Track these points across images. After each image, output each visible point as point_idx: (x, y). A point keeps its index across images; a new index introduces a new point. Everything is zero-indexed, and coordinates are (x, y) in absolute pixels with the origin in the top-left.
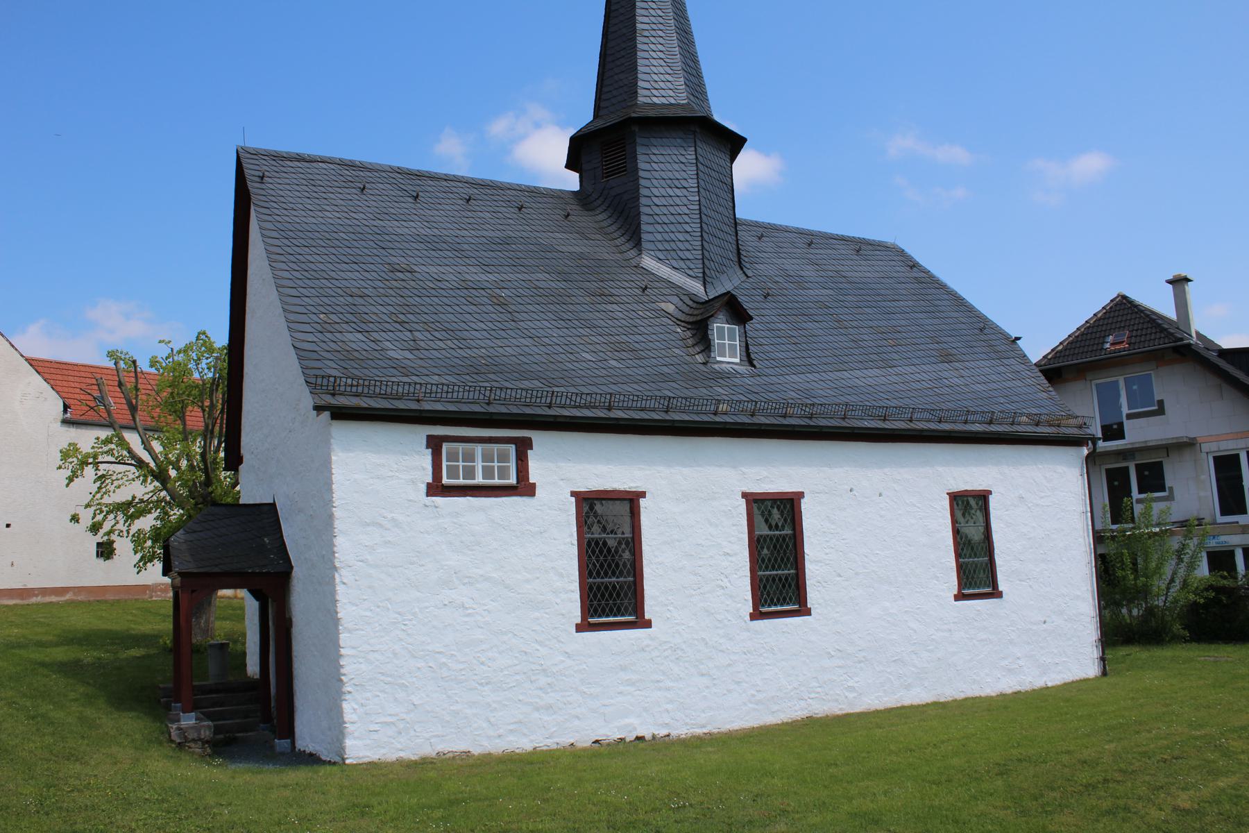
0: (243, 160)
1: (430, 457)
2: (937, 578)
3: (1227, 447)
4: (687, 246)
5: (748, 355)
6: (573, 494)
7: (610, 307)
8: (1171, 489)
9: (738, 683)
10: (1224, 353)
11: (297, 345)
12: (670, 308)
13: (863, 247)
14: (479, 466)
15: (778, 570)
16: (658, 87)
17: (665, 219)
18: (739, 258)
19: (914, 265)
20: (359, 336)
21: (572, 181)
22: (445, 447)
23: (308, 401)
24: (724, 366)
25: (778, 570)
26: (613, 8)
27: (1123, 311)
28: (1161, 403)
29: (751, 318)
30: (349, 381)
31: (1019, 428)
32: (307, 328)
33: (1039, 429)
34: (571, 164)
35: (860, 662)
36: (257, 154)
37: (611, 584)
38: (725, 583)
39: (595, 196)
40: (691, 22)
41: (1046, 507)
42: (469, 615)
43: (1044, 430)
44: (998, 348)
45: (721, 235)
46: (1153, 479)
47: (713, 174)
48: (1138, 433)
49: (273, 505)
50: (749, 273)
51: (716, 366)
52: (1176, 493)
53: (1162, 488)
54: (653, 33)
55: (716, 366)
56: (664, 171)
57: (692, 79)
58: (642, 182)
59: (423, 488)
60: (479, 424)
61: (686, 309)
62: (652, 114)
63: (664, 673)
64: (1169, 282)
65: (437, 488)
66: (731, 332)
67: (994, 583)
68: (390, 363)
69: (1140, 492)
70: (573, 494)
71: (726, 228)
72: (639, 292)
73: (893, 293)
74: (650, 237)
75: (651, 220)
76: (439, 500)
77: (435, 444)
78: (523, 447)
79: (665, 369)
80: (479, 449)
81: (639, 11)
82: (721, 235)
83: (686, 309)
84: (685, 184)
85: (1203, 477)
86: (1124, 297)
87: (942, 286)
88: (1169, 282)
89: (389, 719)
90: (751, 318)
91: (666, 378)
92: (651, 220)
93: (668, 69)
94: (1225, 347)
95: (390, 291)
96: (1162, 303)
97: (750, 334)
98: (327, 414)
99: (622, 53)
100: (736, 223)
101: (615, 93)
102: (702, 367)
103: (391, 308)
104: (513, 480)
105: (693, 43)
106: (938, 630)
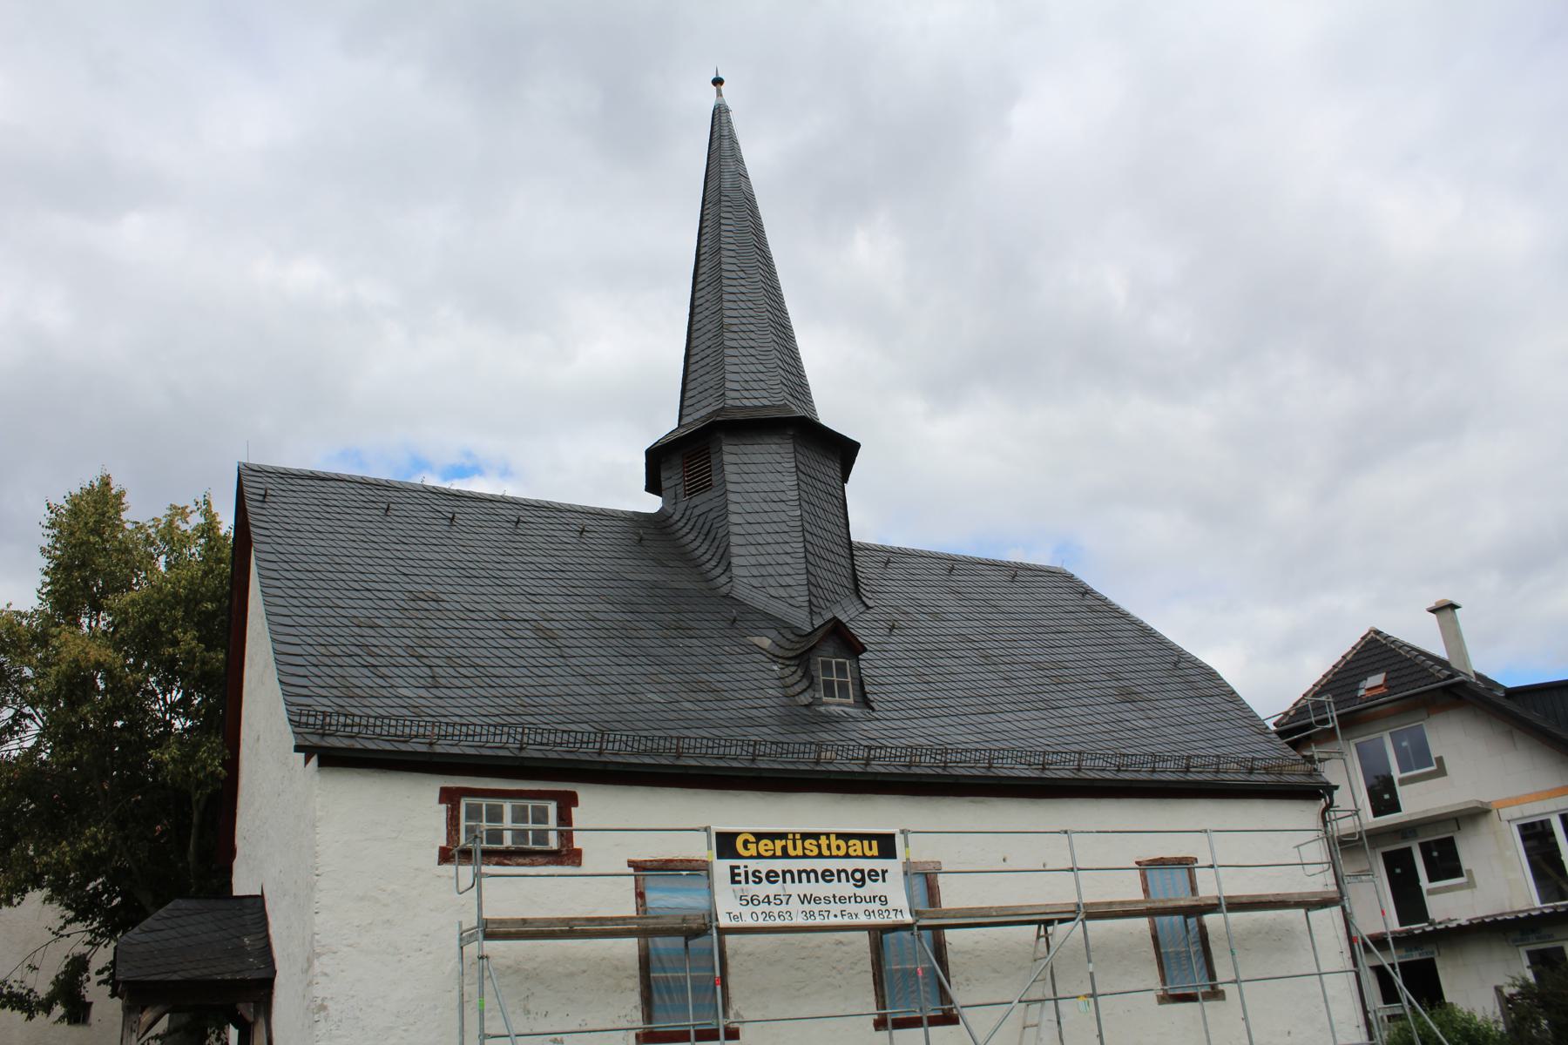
3: (1533, 811)
7: (687, 642)
8: (1470, 872)
10: (1512, 693)
11: (285, 679)
12: (766, 643)
18: (857, 586)
19: (1086, 592)
21: (652, 504)
22: (464, 802)
23: (291, 741)
27: (1375, 651)
28: (1440, 760)
29: (865, 650)
30: (342, 719)
31: (1226, 777)
32: (299, 661)
33: (1253, 777)
34: (653, 486)
43: (1259, 778)
44: (1199, 685)
45: (832, 557)
46: (1446, 863)
47: (819, 485)
48: (1417, 801)
49: (262, 897)
51: (822, 709)
52: (1477, 878)
53: (1456, 871)
55: (822, 709)
61: (787, 645)
62: (740, 416)
64: (1433, 611)
69: (1431, 880)
73: (1050, 618)
74: (742, 561)
77: (449, 797)
78: (567, 802)
80: (507, 807)
82: (832, 557)
83: (787, 645)
85: (1508, 853)
86: (1378, 633)
87: (1125, 616)
88: (1433, 611)
91: (753, 722)
94: (1509, 686)
95: (410, 622)
96: (1425, 636)
102: (805, 711)
103: (408, 641)
104: (554, 843)
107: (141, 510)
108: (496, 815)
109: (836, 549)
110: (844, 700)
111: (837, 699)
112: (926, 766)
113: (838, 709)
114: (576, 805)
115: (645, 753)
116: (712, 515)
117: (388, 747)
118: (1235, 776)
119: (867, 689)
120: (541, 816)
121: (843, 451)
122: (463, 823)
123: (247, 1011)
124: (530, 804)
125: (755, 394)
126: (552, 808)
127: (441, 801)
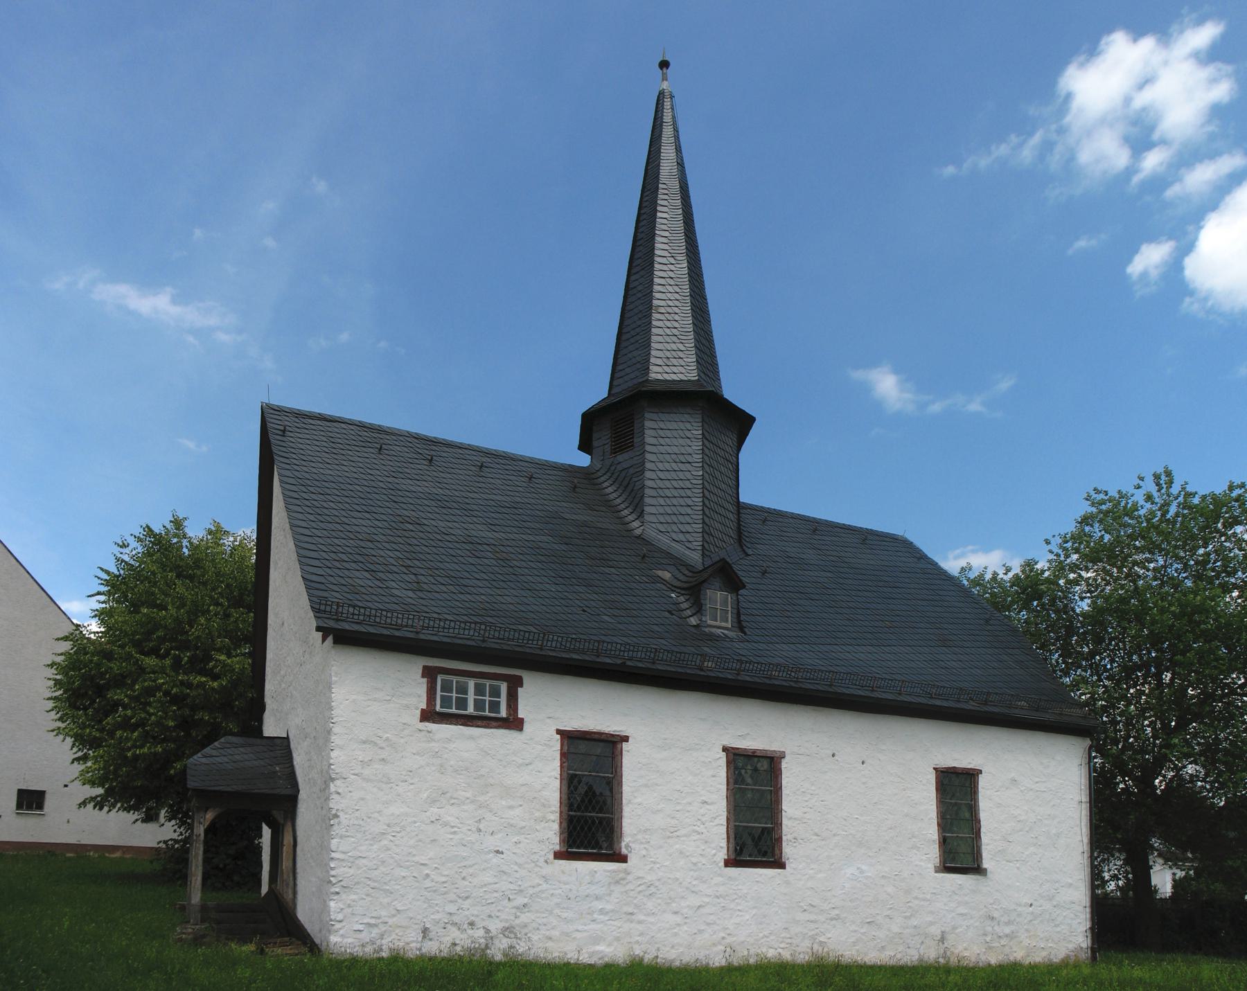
0: (266, 415)
1: (425, 686)
4: (688, 519)
5: (739, 622)
6: (559, 732)
7: (607, 570)
9: (708, 924)
12: (667, 575)
13: (870, 537)
14: (471, 697)
15: (755, 839)
16: (671, 363)
17: (668, 493)
24: (713, 630)
26: (631, 286)
35: (832, 919)
36: (279, 410)
37: (590, 826)
38: (701, 828)
39: (603, 471)
40: (709, 301)
41: (1039, 794)
42: (455, 833)
45: (722, 511)
50: (750, 552)
54: (669, 310)
56: (672, 444)
57: (705, 357)
58: (648, 456)
59: (722, 864)
60: (472, 667)
63: (636, 906)
65: (428, 715)
66: (725, 602)
67: (976, 855)
68: (393, 600)
70: (559, 732)
71: (729, 498)
72: (637, 564)
74: (652, 510)
75: (653, 493)
77: (430, 673)
79: (656, 628)
81: (656, 288)
82: (722, 511)
89: (373, 921)
90: (744, 587)
92: (653, 493)
93: (672, 261)
97: (742, 604)
98: (330, 639)
99: (638, 330)
101: (628, 370)
102: (693, 630)
104: (503, 713)
106: (916, 898)
107: (557, 848)
108: (463, 690)
114: (521, 686)
120: (496, 692)
121: (741, 423)
122: (439, 693)
123: (278, 815)
124: (488, 683)
125: (674, 369)
126: (504, 687)
127: (423, 676)
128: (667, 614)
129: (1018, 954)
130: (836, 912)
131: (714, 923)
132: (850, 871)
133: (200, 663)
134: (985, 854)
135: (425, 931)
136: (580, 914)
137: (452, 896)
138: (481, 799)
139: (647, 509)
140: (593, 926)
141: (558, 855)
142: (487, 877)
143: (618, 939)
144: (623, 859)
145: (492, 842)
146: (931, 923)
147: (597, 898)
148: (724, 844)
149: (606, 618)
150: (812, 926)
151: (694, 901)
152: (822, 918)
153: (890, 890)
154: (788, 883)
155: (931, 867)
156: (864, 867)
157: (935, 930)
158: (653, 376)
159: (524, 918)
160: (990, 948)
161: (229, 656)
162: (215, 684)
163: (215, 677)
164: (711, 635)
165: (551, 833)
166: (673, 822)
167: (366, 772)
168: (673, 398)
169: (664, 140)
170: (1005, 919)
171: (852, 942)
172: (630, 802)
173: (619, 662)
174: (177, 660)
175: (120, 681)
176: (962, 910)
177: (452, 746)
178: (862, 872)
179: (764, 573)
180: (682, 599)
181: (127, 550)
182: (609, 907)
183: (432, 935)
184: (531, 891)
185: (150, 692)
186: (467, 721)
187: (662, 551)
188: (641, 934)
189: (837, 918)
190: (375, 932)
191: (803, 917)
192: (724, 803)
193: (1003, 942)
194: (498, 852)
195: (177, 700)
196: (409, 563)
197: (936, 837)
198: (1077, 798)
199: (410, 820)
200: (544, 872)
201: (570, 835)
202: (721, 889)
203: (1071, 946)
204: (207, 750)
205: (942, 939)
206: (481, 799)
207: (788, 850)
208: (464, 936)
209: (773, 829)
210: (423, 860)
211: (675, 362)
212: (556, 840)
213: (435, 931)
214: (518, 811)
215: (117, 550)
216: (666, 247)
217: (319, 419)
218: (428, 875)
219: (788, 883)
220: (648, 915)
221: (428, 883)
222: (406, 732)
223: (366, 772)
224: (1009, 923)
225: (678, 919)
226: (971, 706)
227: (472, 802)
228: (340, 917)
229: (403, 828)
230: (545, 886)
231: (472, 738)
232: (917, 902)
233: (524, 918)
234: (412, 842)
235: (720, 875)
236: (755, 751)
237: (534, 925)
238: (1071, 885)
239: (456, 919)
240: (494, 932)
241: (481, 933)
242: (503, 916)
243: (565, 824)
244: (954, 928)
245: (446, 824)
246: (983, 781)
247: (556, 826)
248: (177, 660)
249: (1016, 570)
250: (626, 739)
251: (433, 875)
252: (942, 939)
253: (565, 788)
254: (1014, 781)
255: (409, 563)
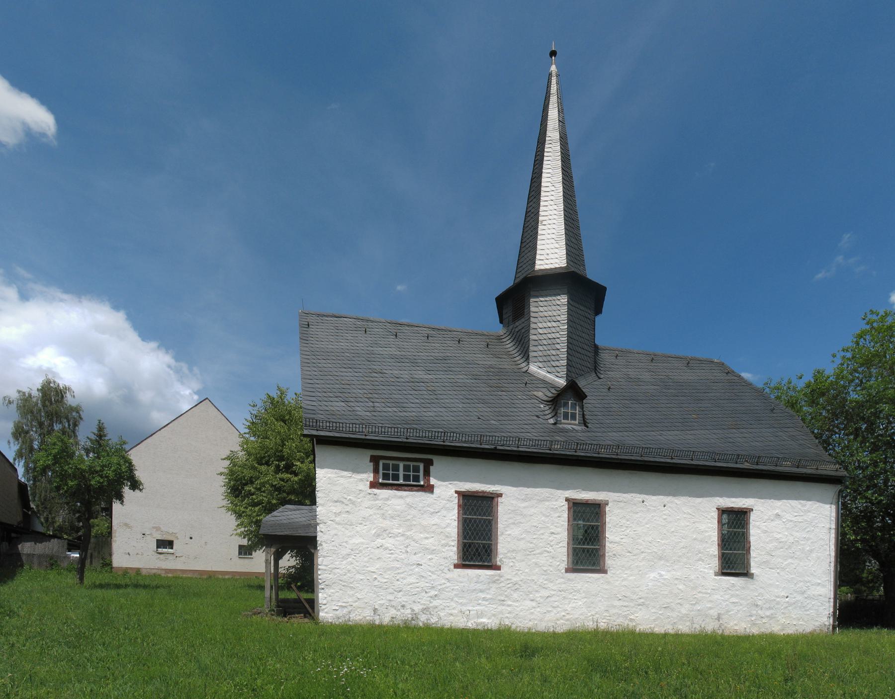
2: (703, 561)
6: (456, 492)
7: (500, 393)
12: (540, 394)
14: (401, 473)
15: (587, 546)
20: (343, 404)
25: (587, 546)
32: (314, 399)
35: (639, 605)
37: (477, 546)
38: (550, 549)
45: (583, 352)
50: (602, 376)
55: (560, 426)
59: (564, 571)
60: (402, 460)
63: (506, 596)
65: (373, 485)
67: (748, 566)
70: (456, 492)
75: (536, 343)
76: (376, 491)
77: (375, 460)
78: (428, 464)
82: (583, 352)
84: (559, 318)
89: (344, 604)
93: (553, 188)
100: (596, 348)
105: (578, 228)
106: (700, 592)
108: (396, 468)
109: (585, 347)
110: (573, 422)
111: (569, 421)
112: (604, 454)
113: (569, 427)
115: (465, 442)
116: (523, 331)
117: (347, 436)
118: (786, 467)
119: (587, 417)
120: (416, 469)
124: (412, 464)
125: (552, 261)
127: (371, 461)
128: (535, 418)
129: (776, 628)
130: (642, 600)
131: (558, 607)
132: (652, 575)
133: (288, 468)
134: (752, 564)
135: (375, 610)
136: (468, 603)
137: (391, 590)
138: (408, 533)
139: (531, 354)
140: (478, 608)
141: (456, 566)
142: (412, 579)
143: (494, 615)
144: (498, 568)
145: (414, 559)
146: (711, 608)
147: (481, 591)
148: (565, 558)
149: (493, 422)
150: (625, 609)
151: (546, 593)
152: (632, 604)
153: (681, 587)
154: (609, 583)
155: (712, 572)
156: (663, 573)
157: (714, 613)
158: (537, 267)
159: (436, 603)
160: (754, 624)
161: (302, 463)
162: (296, 479)
163: (296, 475)
164: (564, 428)
165: (452, 552)
166: (531, 545)
167: (337, 519)
168: (550, 282)
169: (551, 106)
170: (767, 605)
171: (648, 620)
172: (502, 534)
173: (493, 447)
174: (278, 466)
175: (251, 481)
176: (734, 600)
177: (389, 502)
178: (661, 575)
179: (609, 388)
180: (547, 408)
181: (256, 408)
182: (488, 596)
183: (379, 613)
184: (439, 587)
185: (263, 484)
186: (399, 487)
187: (540, 380)
188: (510, 613)
189: (642, 604)
190: (345, 611)
191: (617, 603)
192: (566, 533)
193: (764, 621)
194: (419, 564)
195: (278, 489)
196: (370, 396)
197: (716, 553)
198: (828, 526)
199: (365, 546)
200: (447, 576)
201: (464, 554)
202: (563, 586)
203: (817, 624)
204: (275, 513)
205: (718, 619)
206: (408, 533)
207: (609, 562)
208: (399, 613)
209: (840, 586)
210: (373, 569)
211: (551, 256)
212: (456, 557)
213: (381, 610)
214: (431, 540)
215: (251, 408)
216: (549, 180)
217: (332, 316)
218: (376, 578)
219: (609, 583)
220: (514, 601)
221: (376, 583)
222: (361, 495)
223: (337, 519)
224: (770, 608)
225: (534, 604)
226: (746, 465)
227: (403, 535)
228: (325, 602)
229: (361, 551)
230: (448, 584)
231: (401, 497)
232: (701, 595)
233: (436, 603)
234: (366, 559)
235: (562, 578)
236: (588, 500)
237: (442, 607)
238: (819, 584)
239: (393, 603)
240: (417, 611)
241: (409, 611)
242: (422, 602)
243: (461, 548)
244: (728, 611)
245: (386, 549)
246: (753, 517)
247: (455, 549)
248: (278, 466)
249: (808, 378)
250: (500, 495)
251: (379, 578)
252: (718, 619)
253: (461, 526)
254: (778, 515)
255: (370, 396)
